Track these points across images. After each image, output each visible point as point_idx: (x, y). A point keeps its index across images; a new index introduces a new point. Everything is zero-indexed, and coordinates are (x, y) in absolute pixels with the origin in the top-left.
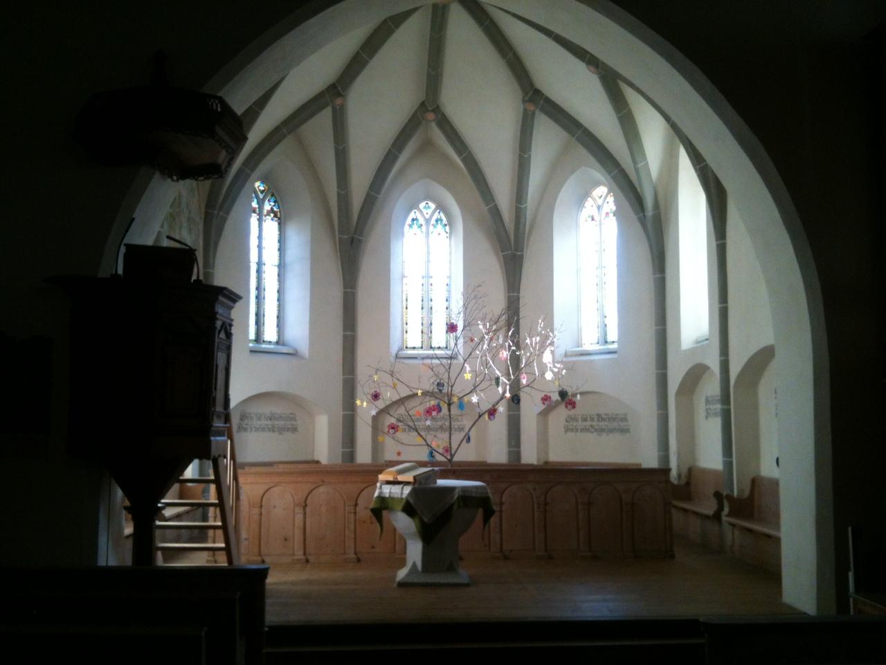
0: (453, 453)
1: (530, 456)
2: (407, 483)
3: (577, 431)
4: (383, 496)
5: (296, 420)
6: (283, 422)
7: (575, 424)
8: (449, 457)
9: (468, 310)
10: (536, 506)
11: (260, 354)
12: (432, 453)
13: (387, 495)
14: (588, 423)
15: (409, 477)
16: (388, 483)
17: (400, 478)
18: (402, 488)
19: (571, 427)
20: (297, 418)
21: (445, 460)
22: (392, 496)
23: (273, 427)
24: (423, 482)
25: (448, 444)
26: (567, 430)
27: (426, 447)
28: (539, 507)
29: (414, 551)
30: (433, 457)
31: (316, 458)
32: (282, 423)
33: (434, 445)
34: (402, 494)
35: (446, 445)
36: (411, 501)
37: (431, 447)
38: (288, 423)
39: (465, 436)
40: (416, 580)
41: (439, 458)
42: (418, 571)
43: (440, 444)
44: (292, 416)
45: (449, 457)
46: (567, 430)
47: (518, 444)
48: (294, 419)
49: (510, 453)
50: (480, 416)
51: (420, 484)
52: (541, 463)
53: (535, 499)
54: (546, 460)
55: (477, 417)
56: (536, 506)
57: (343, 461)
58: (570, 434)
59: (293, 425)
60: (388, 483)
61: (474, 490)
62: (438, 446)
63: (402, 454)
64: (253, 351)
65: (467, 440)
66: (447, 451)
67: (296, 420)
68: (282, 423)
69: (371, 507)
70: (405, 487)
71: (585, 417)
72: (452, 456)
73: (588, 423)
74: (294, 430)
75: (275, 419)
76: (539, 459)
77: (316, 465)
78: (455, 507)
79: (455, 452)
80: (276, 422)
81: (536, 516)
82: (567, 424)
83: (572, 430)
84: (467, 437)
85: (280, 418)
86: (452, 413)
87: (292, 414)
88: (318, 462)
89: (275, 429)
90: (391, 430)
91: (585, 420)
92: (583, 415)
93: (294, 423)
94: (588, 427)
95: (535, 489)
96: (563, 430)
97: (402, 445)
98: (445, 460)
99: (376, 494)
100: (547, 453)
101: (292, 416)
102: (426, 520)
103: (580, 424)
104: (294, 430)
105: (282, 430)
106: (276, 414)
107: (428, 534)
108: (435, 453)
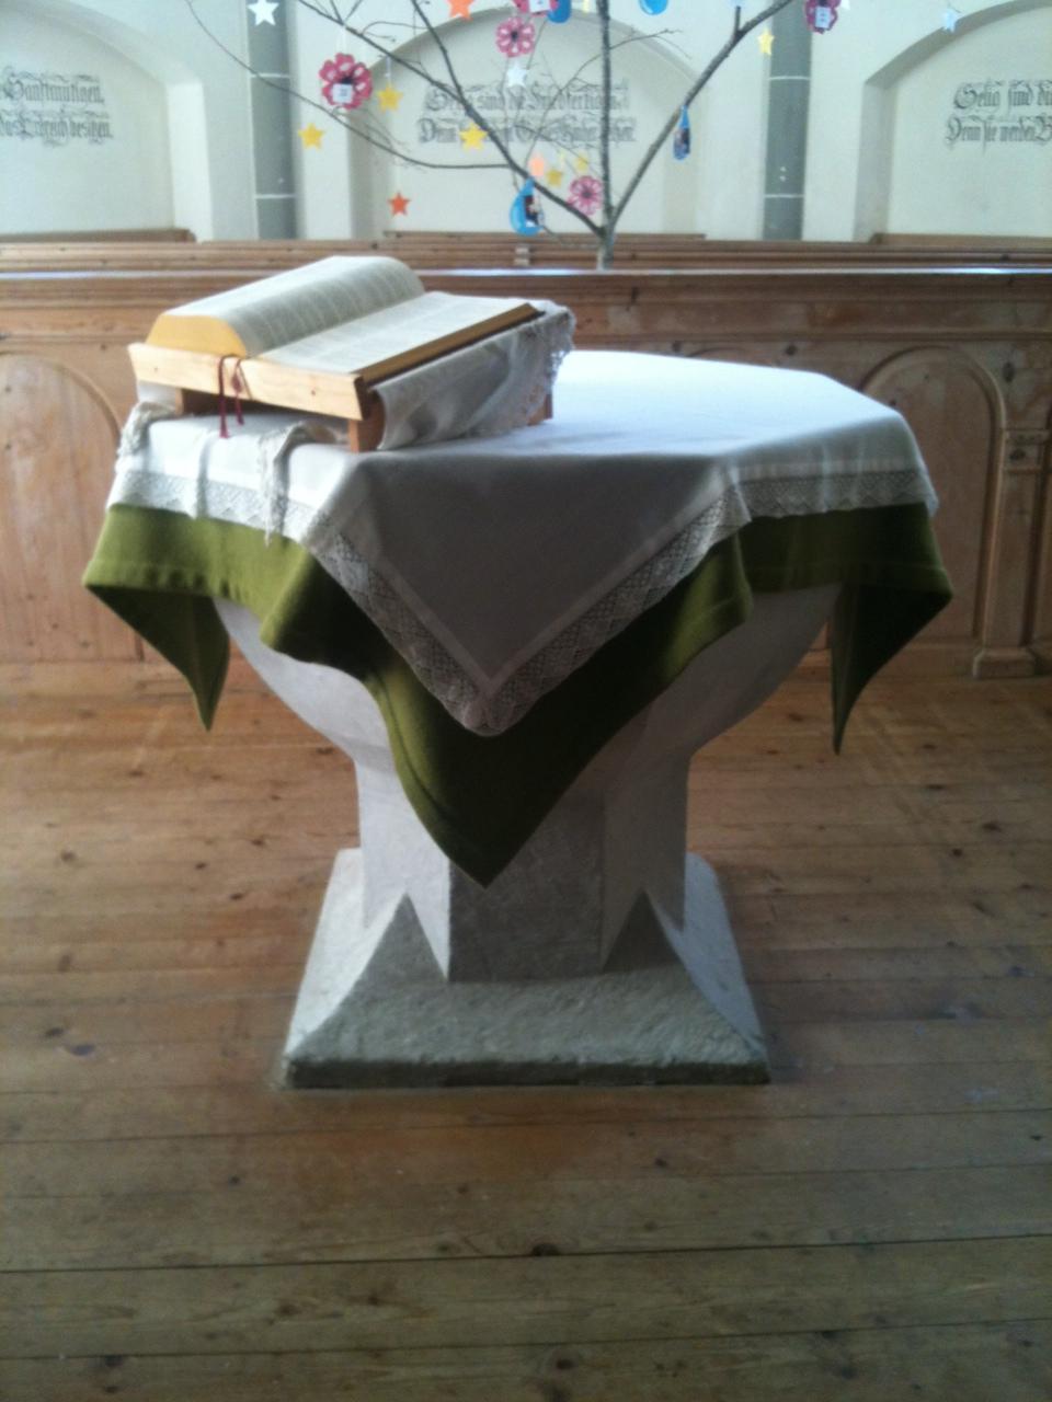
0: (615, 200)
1: (830, 217)
2: (315, 428)
3: (989, 134)
4: (158, 501)
5: (101, 101)
6: (55, 106)
7: (984, 112)
8: (598, 218)
9: (541, 401)
10: (1003, 451)
11: (478, 163)
12: (529, 200)
13: (187, 504)
14: (1033, 110)
15: (320, 375)
16: (197, 405)
17: (265, 379)
18: (283, 459)
19: (971, 124)
20: (104, 93)
21: (580, 227)
22: (216, 511)
23: (22, 121)
24: (444, 417)
25: (597, 172)
26: (958, 132)
27: (507, 172)
28: (1017, 456)
29: (386, 877)
30: (533, 216)
31: (180, 223)
32: (50, 107)
33: (539, 173)
34: (281, 505)
35: (583, 172)
36: (349, 574)
37: (524, 174)
38: (73, 106)
39: (669, 128)
40: (410, 1047)
41: (559, 221)
42: (430, 970)
43: (562, 166)
44: (87, 85)
45: (598, 218)
46: (958, 132)
47: (796, 181)
48: (94, 94)
49: (770, 207)
50: (739, 34)
51: (421, 431)
52: (865, 237)
53: (1003, 421)
54: (878, 230)
55: (727, 35)
56: (1003, 451)
57: (265, 231)
58: (966, 147)
59: (92, 114)
60: (197, 405)
61: (827, 467)
62: (556, 175)
63: (409, 207)
64: (275, 45)
65: (677, 146)
66: (587, 195)
67: (101, 101)
68: (50, 107)
69: (95, 568)
70: (303, 456)
71: (1021, 88)
72: (612, 212)
73: (1033, 110)
74: (99, 131)
75: (24, 90)
76: (858, 226)
77: (171, 250)
78: (697, 617)
79: (625, 200)
80: (32, 106)
81: (1002, 484)
82: (959, 113)
83: (973, 134)
84: (677, 128)
85: (43, 88)
86: (598, 113)
87: (84, 77)
88: (184, 236)
89: (29, 128)
90: (337, 89)
91: (1021, 99)
92: (1015, 84)
93: (94, 107)
94: (1027, 123)
95: (1009, 374)
96: (945, 131)
97: (412, 169)
98: (580, 227)
99: (116, 495)
100: (883, 208)
101: (87, 85)
102: (465, 717)
103: (1005, 114)
104: (99, 131)
105: (53, 131)
106: (28, 76)
107: (478, 797)
108: (541, 202)
